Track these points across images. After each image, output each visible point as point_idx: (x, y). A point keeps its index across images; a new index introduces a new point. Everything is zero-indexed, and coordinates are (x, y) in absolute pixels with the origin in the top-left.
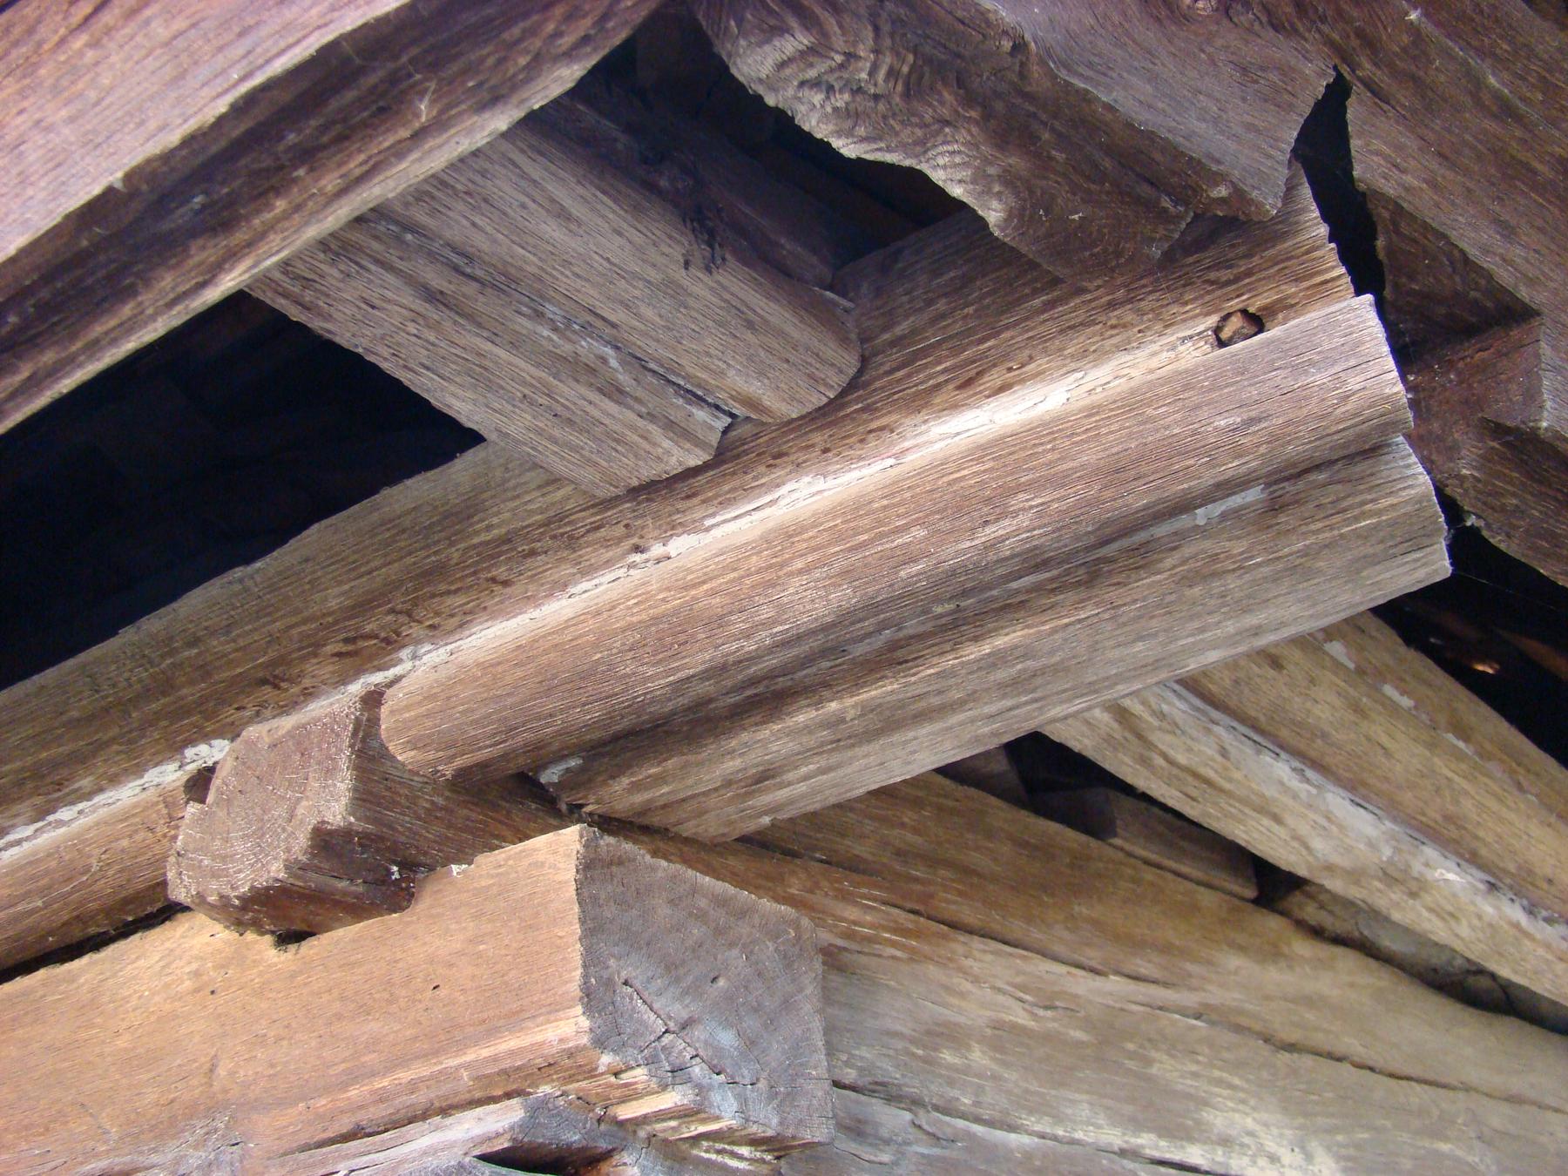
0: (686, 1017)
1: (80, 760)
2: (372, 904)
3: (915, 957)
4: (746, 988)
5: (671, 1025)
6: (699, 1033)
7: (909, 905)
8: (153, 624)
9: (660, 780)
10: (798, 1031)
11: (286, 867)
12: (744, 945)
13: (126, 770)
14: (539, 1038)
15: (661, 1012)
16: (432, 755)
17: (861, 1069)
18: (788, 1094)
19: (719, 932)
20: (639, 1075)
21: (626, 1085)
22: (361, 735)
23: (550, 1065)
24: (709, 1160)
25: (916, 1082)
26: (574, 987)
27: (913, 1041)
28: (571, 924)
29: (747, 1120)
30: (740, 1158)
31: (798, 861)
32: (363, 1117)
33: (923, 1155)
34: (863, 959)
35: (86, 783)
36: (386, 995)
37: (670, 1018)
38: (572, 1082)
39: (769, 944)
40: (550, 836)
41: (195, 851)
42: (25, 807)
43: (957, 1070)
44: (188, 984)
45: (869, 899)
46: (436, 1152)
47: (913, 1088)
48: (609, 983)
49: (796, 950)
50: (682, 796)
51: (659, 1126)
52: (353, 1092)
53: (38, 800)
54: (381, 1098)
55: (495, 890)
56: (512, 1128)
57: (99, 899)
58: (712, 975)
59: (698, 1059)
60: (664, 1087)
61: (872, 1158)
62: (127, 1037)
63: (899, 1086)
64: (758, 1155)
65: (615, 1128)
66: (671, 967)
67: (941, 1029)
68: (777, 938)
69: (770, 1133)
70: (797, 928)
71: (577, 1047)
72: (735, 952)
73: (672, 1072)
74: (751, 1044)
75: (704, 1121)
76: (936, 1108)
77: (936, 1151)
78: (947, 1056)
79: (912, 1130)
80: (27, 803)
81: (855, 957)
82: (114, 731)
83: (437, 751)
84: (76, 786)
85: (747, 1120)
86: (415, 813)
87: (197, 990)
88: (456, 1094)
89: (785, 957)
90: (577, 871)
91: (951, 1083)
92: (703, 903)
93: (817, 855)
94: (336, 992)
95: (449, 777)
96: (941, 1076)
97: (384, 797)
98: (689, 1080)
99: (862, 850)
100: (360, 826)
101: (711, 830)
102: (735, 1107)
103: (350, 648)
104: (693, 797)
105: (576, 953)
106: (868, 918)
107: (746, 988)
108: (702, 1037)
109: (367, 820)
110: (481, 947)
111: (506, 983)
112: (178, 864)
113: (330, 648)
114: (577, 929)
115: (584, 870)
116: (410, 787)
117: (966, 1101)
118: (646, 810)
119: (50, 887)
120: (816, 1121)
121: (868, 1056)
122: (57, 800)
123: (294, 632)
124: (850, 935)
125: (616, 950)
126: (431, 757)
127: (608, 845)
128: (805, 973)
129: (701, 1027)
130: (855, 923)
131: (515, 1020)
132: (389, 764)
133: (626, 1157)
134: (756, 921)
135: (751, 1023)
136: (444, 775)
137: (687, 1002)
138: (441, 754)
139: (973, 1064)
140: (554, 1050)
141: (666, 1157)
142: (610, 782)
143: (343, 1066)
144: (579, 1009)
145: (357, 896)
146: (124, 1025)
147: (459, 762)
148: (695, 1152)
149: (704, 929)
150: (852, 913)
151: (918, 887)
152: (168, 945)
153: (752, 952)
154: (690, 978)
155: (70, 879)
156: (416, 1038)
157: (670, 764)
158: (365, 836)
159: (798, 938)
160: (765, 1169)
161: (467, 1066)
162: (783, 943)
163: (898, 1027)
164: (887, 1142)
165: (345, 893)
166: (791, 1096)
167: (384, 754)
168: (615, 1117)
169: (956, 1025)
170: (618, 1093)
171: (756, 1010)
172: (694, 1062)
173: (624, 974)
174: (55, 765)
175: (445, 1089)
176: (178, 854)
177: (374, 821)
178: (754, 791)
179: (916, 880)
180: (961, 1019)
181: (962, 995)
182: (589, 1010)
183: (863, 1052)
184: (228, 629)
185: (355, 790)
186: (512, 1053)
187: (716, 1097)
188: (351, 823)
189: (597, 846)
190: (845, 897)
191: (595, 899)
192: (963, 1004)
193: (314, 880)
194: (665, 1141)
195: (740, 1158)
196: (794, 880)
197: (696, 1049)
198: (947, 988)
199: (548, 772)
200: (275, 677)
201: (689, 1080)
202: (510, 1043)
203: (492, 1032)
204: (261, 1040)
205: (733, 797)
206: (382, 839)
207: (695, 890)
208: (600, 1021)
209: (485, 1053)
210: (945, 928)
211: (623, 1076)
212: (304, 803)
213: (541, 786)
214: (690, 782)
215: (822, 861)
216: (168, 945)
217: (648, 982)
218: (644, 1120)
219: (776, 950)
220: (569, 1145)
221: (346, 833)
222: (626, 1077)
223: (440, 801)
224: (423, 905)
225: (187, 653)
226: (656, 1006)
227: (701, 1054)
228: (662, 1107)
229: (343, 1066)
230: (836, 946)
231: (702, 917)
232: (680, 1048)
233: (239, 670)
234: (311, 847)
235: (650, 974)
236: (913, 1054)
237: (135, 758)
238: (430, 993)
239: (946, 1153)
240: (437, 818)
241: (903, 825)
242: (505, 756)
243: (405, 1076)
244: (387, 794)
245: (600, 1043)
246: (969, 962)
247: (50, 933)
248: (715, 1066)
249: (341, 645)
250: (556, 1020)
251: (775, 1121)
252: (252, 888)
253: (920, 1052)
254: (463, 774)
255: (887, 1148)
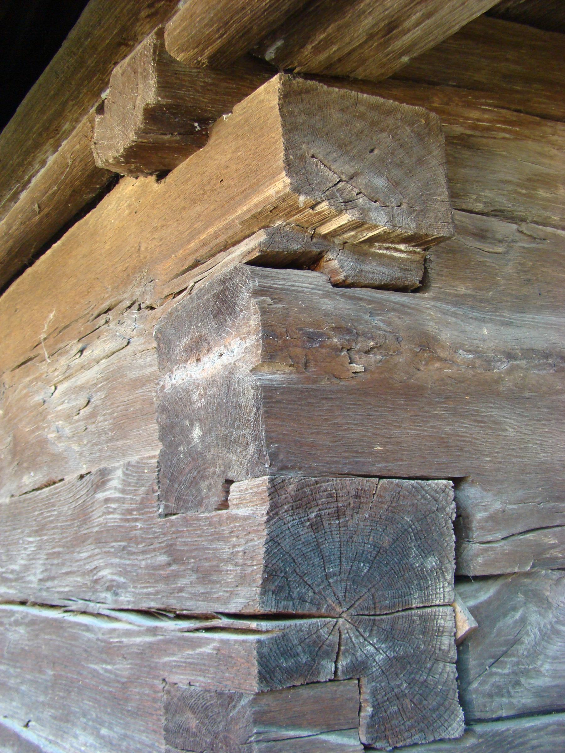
0: (353, 172)
1: (59, 114)
2: (186, 145)
3: (519, 137)
4: (393, 154)
5: (344, 177)
6: (361, 180)
7: (513, 107)
8: (73, 34)
9: (327, 43)
10: (428, 176)
11: (136, 133)
12: (391, 130)
13: (80, 114)
14: (267, 194)
15: (336, 171)
16: (192, 53)
17: (485, 203)
18: (422, 211)
19: (373, 124)
20: (324, 206)
21: (319, 213)
22: (157, 53)
23: (275, 208)
24: (382, 254)
25: (522, 209)
26: (280, 162)
27: (518, 185)
28: (278, 128)
29: (394, 226)
30: (401, 251)
31: (438, 88)
32: (197, 255)
33: (524, 248)
34: (484, 141)
35: (67, 126)
36: (201, 192)
37: (342, 173)
38: (291, 216)
39: (408, 128)
40: (266, 84)
41: (101, 139)
42: (47, 147)
43: (549, 201)
44: (127, 212)
45: (486, 105)
46: (227, 265)
47: (520, 212)
48: (302, 157)
49: (426, 131)
50: (347, 50)
51: (346, 236)
52: (192, 245)
53: (52, 141)
54: (204, 244)
55: (242, 122)
56: (259, 245)
57: (77, 179)
58: (370, 148)
59: (361, 195)
60: (340, 212)
61: (491, 250)
62: (109, 243)
63: (511, 211)
64: (411, 249)
65: (322, 240)
66: (342, 146)
67: (537, 178)
68: (413, 124)
69: (410, 233)
70: (427, 118)
71: (285, 195)
72: (384, 134)
73: (345, 202)
74: (396, 184)
75: (369, 229)
76: (533, 222)
77: (534, 245)
78: (542, 193)
79: (518, 234)
80: (48, 144)
81: (479, 140)
82: (67, 94)
83: (194, 49)
84: (64, 129)
85: (394, 226)
86: (195, 89)
87: (130, 214)
88: (236, 234)
89: (419, 135)
90: (280, 99)
91: (545, 208)
92: (362, 109)
93: (450, 83)
94: (182, 196)
95: (207, 64)
96: (538, 204)
97: (176, 84)
98: (356, 206)
99: (481, 77)
100: (164, 102)
101: (374, 72)
102: (386, 219)
103: (153, 10)
104: (354, 50)
105: (281, 144)
106: (486, 116)
107: (393, 154)
108: (364, 182)
109: (167, 97)
110: (239, 154)
111: (250, 169)
112: (96, 149)
113: (143, 14)
114: (281, 130)
115: (283, 98)
116: (191, 76)
117: (555, 218)
118: (330, 66)
119: (57, 179)
120: (440, 224)
121: (490, 195)
122: (59, 139)
123: (125, 11)
124: (475, 128)
125: (305, 139)
126: (192, 54)
127: (298, 82)
128: (433, 143)
129: (363, 177)
130: (478, 120)
131: (256, 188)
132: (176, 65)
133: (330, 256)
134: (399, 116)
135: (397, 173)
136: (203, 63)
137: (353, 164)
138: (196, 50)
139: (559, 197)
140: (274, 199)
141: (354, 253)
142: (302, 50)
143: (188, 232)
144: (284, 173)
145: (177, 142)
146: (107, 238)
147: (207, 53)
148: (373, 250)
149: (363, 123)
150: (475, 114)
151: (518, 96)
152: (118, 196)
153: (396, 133)
154: (355, 151)
155: (63, 173)
156: (215, 209)
157: (330, 29)
158: (169, 107)
159: (427, 124)
160: (417, 257)
161: (238, 217)
162: (416, 127)
163: (509, 178)
164: (501, 241)
165: (170, 142)
166: (424, 212)
167: (172, 61)
168: (320, 234)
169: (548, 174)
170: (316, 219)
171: (399, 166)
172: (359, 196)
173: (311, 152)
174: (50, 121)
175: (231, 232)
176: (95, 143)
177: (172, 97)
178: (389, 39)
179: (517, 92)
180: (552, 172)
181: (551, 157)
182: (289, 173)
183: (487, 193)
184: (99, 23)
185: (158, 82)
186: (257, 205)
187: (373, 215)
188: (159, 101)
189: (291, 84)
190: (469, 105)
191: (291, 113)
192: (552, 162)
193: (152, 137)
194: (353, 245)
195: (401, 251)
196: (436, 99)
197: (360, 189)
198: (540, 154)
199: (268, 53)
200: (124, 39)
201: (356, 206)
202: (255, 200)
203: (246, 195)
204: (156, 229)
205: (378, 46)
206: (178, 106)
207: (357, 102)
208: (297, 178)
209: (245, 209)
210: (538, 119)
211: (317, 208)
212: (139, 98)
213: (267, 63)
214: (347, 39)
215: (454, 86)
216: (118, 196)
217: (327, 154)
218: (334, 234)
219: (412, 131)
220: (295, 251)
221: (159, 107)
222: (319, 208)
223: (209, 81)
224: (212, 141)
225: (86, 43)
226: (332, 168)
227: (363, 191)
228: (342, 224)
229: (188, 232)
230: (466, 134)
231: (362, 116)
232: (350, 190)
233: (107, 41)
234: (145, 119)
235: (328, 150)
236: (520, 193)
237: (82, 106)
238: (219, 185)
239: (540, 246)
240: (208, 90)
241: (507, 60)
242: (229, 43)
243: (212, 230)
244: (178, 81)
245: (297, 190)
246: (555, 138)
247: (68, 202)
248: (372, 198)
249: (147, 9)
250: (274, 182)
251: (413, 226)
252: (125, 149)
253: (524, 191)
254: (212, 58)
255: (501, 245)
